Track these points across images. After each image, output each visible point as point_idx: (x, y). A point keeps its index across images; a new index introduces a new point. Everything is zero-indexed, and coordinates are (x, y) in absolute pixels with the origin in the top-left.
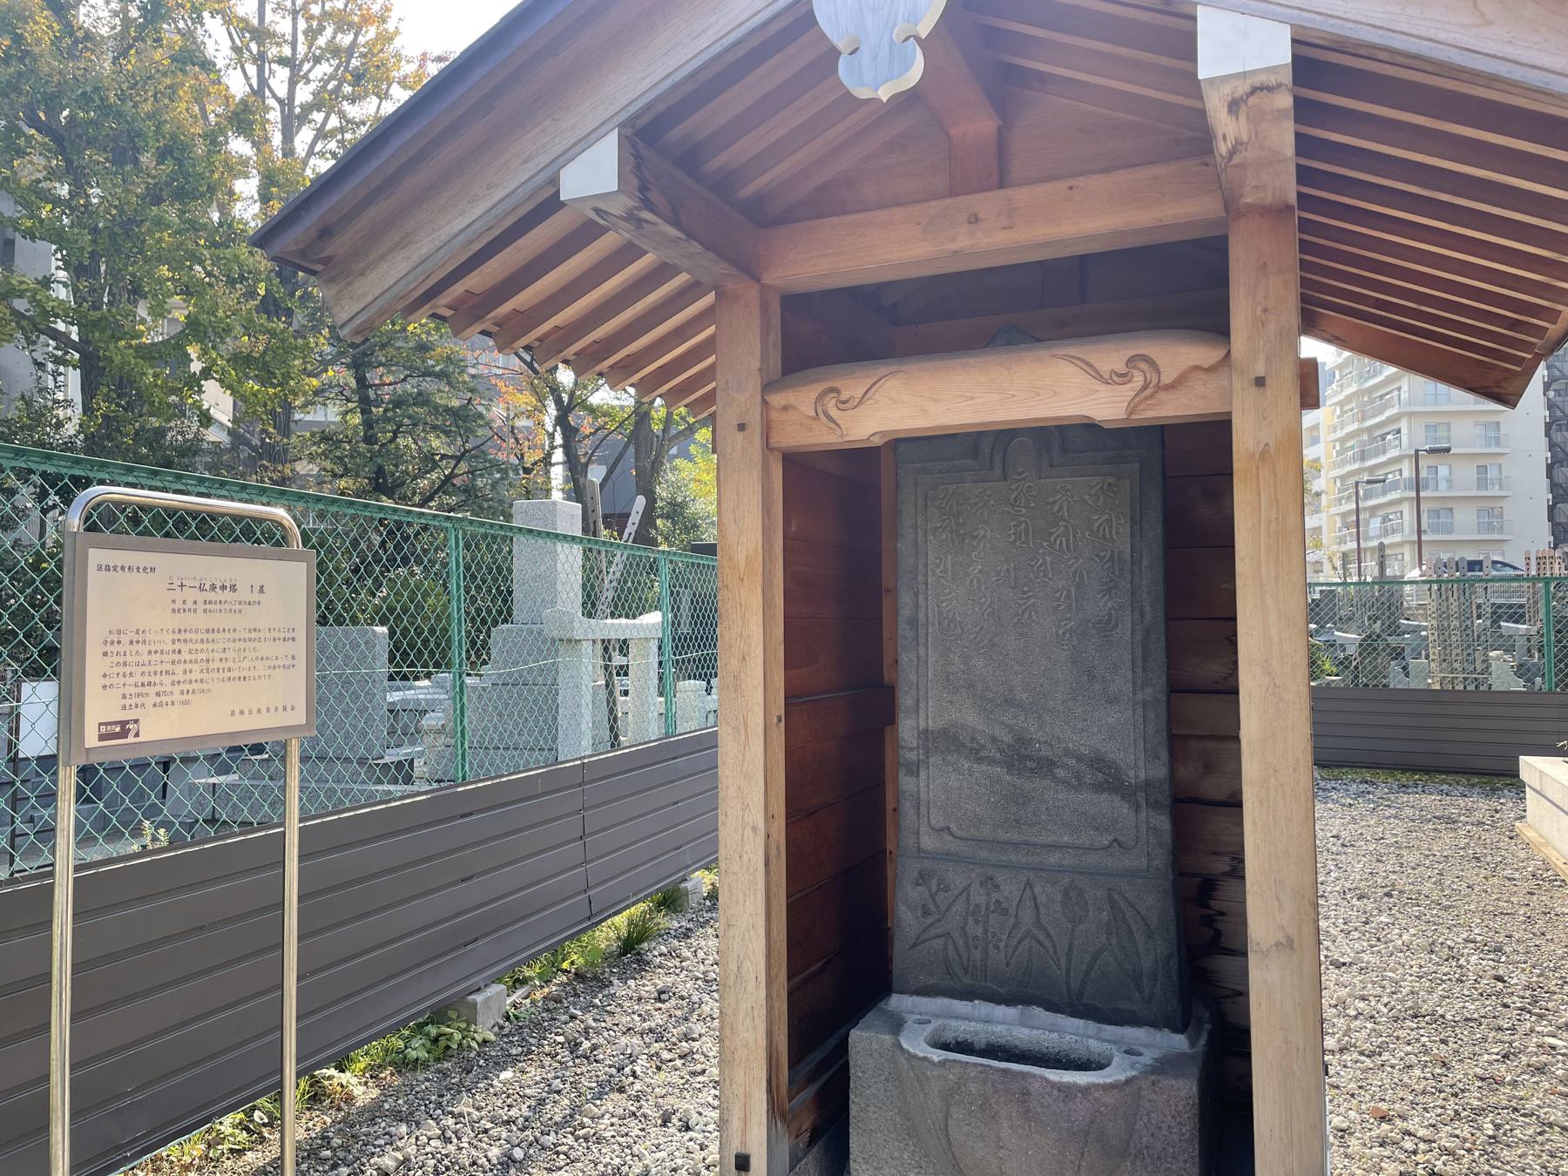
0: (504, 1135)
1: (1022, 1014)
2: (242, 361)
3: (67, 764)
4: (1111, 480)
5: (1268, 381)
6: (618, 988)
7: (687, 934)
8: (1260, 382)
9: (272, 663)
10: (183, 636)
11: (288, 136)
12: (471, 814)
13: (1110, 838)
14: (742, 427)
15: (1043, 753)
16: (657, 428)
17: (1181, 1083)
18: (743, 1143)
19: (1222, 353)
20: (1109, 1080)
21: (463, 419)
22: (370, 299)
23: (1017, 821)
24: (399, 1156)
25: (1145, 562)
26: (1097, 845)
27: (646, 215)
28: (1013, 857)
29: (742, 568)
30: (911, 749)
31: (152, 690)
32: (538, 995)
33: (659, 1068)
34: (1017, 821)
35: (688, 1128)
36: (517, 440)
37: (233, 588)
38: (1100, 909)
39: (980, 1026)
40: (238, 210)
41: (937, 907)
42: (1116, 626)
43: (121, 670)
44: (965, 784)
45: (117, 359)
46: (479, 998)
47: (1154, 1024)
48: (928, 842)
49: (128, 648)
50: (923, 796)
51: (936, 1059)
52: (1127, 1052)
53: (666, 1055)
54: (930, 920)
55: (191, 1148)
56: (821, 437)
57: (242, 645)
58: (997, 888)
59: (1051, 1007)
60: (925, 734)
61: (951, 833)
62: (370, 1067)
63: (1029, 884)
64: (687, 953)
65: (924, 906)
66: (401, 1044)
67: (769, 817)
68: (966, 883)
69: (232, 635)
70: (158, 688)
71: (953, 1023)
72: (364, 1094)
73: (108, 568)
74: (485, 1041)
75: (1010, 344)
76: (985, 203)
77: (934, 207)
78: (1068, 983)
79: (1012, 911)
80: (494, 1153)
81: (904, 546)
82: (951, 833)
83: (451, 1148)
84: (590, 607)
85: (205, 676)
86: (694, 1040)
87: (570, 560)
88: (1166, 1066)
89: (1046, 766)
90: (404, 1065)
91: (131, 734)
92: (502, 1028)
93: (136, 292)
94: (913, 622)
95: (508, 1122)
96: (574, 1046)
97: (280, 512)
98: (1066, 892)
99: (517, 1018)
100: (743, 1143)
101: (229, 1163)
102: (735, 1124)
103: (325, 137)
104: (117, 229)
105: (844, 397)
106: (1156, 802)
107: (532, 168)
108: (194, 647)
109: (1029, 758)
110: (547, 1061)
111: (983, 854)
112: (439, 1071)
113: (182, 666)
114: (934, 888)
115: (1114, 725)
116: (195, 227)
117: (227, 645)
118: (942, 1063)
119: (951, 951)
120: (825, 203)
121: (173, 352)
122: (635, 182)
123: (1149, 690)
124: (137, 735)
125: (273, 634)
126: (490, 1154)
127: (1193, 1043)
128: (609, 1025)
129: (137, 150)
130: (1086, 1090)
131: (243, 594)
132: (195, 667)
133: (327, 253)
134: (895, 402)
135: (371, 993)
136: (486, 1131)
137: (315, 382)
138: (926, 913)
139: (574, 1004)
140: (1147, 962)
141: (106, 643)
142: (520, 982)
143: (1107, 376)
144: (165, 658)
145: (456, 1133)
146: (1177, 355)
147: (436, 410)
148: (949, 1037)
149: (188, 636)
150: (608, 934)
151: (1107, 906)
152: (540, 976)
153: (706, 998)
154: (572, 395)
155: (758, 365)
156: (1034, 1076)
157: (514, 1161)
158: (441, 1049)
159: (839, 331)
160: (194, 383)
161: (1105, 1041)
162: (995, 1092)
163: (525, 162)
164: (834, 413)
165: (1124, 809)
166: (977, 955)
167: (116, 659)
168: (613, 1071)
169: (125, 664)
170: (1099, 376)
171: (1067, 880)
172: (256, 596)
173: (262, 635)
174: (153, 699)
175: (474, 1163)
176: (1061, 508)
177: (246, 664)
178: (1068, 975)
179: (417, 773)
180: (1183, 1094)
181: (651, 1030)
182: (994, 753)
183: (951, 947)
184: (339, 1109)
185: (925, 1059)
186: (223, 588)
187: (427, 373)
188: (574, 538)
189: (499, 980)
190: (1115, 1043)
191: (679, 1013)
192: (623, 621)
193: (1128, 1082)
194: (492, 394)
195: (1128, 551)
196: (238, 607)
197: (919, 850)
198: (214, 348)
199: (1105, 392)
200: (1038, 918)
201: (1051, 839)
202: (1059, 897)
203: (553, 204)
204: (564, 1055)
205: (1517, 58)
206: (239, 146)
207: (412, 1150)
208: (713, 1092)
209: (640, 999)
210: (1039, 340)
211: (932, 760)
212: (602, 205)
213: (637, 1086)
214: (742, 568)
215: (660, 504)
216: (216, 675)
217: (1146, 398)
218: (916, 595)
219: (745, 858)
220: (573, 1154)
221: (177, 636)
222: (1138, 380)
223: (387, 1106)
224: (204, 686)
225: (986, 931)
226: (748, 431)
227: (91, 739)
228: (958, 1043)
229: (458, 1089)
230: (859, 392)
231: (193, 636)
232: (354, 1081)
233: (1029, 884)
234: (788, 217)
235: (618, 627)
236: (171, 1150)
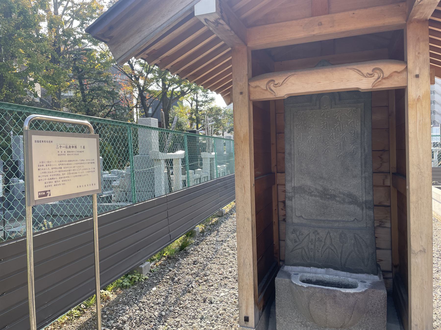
0: (158, 308)
1: (326, 271)
2: (46, 77)
3: (29, 205)
4: (354, 109)
5: (420, 76)
6: (181, 261)
7: (197, 244)
8: (417, 76)
9: (88, 171)
10: (62, 163)
11: (56, 9)
12: (138, 213)
13: (354, 218)
14: (241, 93)
16: (168, 97)
17: (381, 291)
18: (247, 313)
19: (403, 67)
20: (358, 292)
21: (112, 95)
22: (127, 50)
24: (127, 316)
25: (366, 134)
26: (350, 220)
27: (221, 21)
29: (242, 138)
30: (290, 193)
31: (53, 181)
32: (158, 264)
33: (199, 285)
35: (211, 303)
36: (127, 101)
37: (76, 147)
39: (314, 275)
40: (41, 31)
41: (299, 240)
42: (356, 154)
43: (44, 174)
44: (307, 203)
45: (9, 77)
46: (143, 266)
47: (368, 273)
48: (295, 220)
49: (46, 167)
50: (294, 206)
51: (305, 286)
52: (361, 282)
53: (200, 281)
54: (297, 244)
55: (64, 318)
56: (268, 96)
57: (79, 165)
58: (318, 234)
59: (336, 269)
60: (294, 188)
61: (303, 218)
62: (113, 289)
63: (329, 233)
64: (199, 250)
66: (121, 281)
67: (252, 215)
69: (76, 162)
70: (55, 180)
71: (305, 274)
72: (113, 297)
73: (38, 141)
74: (145, 279)
75: (323, 66)
76: (324, 19)
77: (307, 20)
78: (341, 261)
80: (156, 313)
82: (303, 218)
83: (143, 313)
84: (162, 149)
85: (69, 175)
86: (208, 276)
87: (155, 136)
88: (374, 286)
89: (333, 197)
90: (123, 287)
91: (48, 195)
92: (150, 274)
93: (13, 56)
94: (290, 154)
95: (158, 304)
96: (173, 279)
97: (86, 122)
99: (153, 271)
100: (247, 313)
101: (75, 321)
102: (244, 308)
103: (67, 10)
104: (7, 37)
105: (276, 83)
107: (184, 5)
108: (65, 166)
109: (328, 194)
110: (165, 284)
112: (133, 288)
113: (62, 173)
114: (298, 234)
115: (355, 184)
116: (31, 36)
117: (75, 165)
118: (308, 288)
119: (304, 253)
120: (267, 20)
121: (23, 75)
122: (220, 10)
123: (367, 173)
124: (50, 195)
125: (88, 162)
126: (155, 314)
127: (380, 279)
128: (182, 272)
129: (11, 13)
130: (354, 294)
131: (79, 149)
132: (66, 173)
133: (111, 35)
134: (293, 84)
135: (113, 267)
136: (152, 307)
137: (68, 83)
139: (169, 266)
141: (39, 166)
142: (152, 260)
143: (365, 75)
144: (57, 170)
145: (143, 308)
146: (389, 68)
147: (104, 92)
148: (304, 278)
149: (63, 163)
150: (176, 244)
152: (158, 258)
153: (208, 263)
154: (143, 87)
155: (247, 73)
156: (337, 291)
157: (163, 316)
158: (133, 282)
159: (268, 62)
160: (32, 84)
161: (353, 278)
162: (325, 296)
163: (182, 2)
164: (273, 88)
165: (358, 210)
166: (312, 254)
167: (42, 171)
168: (186, 286)
169: (45, 172)
170: (363, 75)
171: (341, 231)
172: (82, 150)
173: (85, 162)
174: (54, 183)
175: (151, 317)
176: (338, 118)
177: (81, 171)
178: (341, 259)
179: (113, 198)
180: (382, 294)
181: (194, 273)
182: (316, 193)
183: (303, 251)
184: (106, 302)
185: (302, 286)
186: (73, 147)
187: (101, 81)
188: (157, 129)
189: (147, 261)
190: (357, 279)
191: (201, 268)
192: (172, 153)
193: (366, 291)
194: (119, 86)
196: (77, 153)
197: (293, 223)
198: (38, 73)
199: (365, 80)
201: (335, 219)
203: (192, 15)
204: (170, 282)
206: (41, 12)
207: (131, 314)
208: (216, 291)
209: (188, 264)
210: (333, 65)
211: (296, 196)
212: (208, 18)
213: (194, 291)
214: (242, 138)
215: (170, 119)
216: (72, 175)
217: (379, 82)
218: (291, 145)
219: (245, 229)
220: (180, 313)
221: (60, 163)
222: (376, 76)
223: (120, 300)
224: (69, 179)
225: (315, 246)
226: (244, 94)
227: (36, 197)
228: (307, 280)
229: (141, 294)
230: (281, 81)
231: (65, 163)
232: (109, 293)
233: (329, 233)
234: (255, 24)
235: (170, 155)
236: (59, 319)
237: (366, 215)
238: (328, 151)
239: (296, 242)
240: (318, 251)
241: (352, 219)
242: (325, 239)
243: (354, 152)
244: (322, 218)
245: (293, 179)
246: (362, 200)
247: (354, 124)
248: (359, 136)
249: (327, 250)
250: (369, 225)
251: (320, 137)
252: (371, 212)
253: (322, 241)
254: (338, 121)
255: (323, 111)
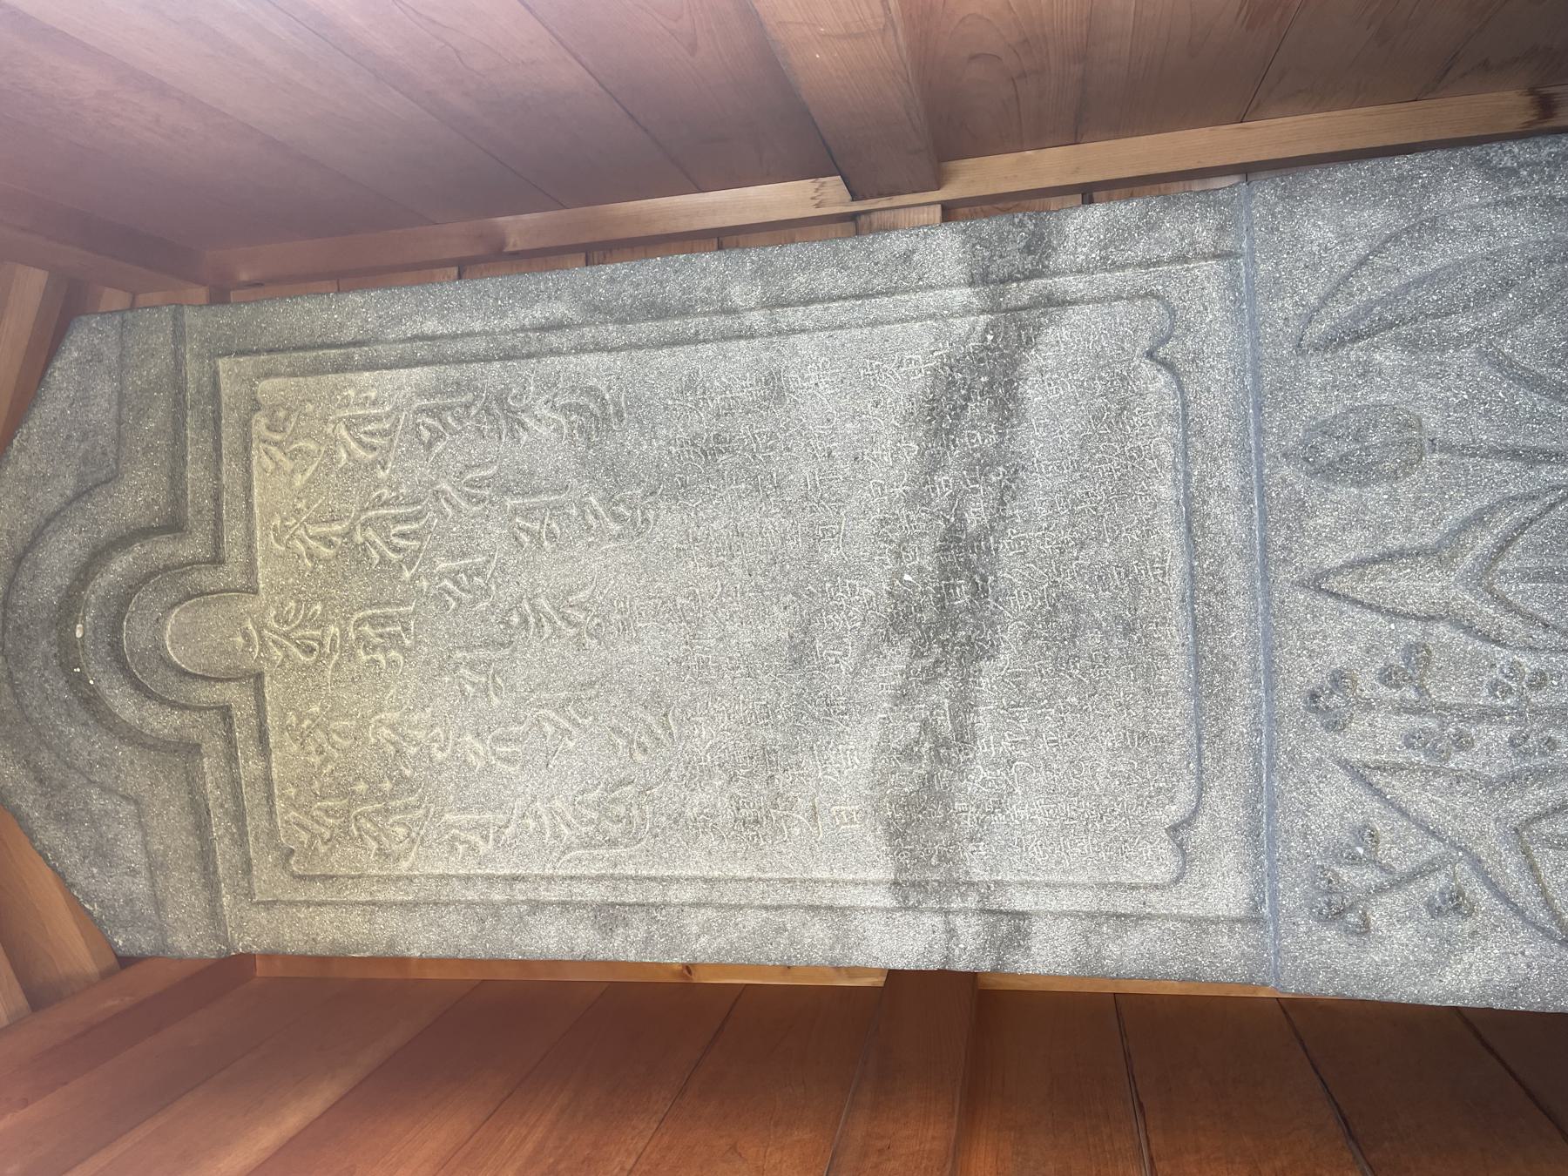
4: (260, 423)
13: (1147, 369)
15: (926, 562)
23: (1129, 630)
25: (431, 326)
26: (1172, 404)
28: (1237, 635)
34: (1129, 630)
38: (1366, 371)
42: (591, 391)
48: (1225, 890)
50: (1085, 901)
54: (1481, 895)
58: (1339, 680)
60: (908, 891)
61: (1188, 822)
63: (1316, 583)
65: (1436, 911)
68: (1342, 778)
79: (1412, 632)
81: (420, 939)
82: (1188, 822)
89: (963, 554)
94: (608, 916)
98: (1329, 472)
106: (1028, 249)
111: (1239, 725)
114: (1371, 877)
138: (1455, 903)
140: (1518, 231)
151: (1355, 352)
171: (1286, 471)
195: (417, 372)
197: (1253, 919)
200: (1422, 552)
201: (1170, 533)
202: (1345, 493)
205: (1192, 164)
211: (979, 874)
218: (537, 906)
225: (1484, 715)
233: (1316, 583)
237: (1108, 265)
238: (581, 607)
239: (1455, 903)
240: (1539, 681)
241: (1163, 378)
242: (1393, 614)
243: (579, 409)
244: (1174, 638)
245: (825, 896)
246: (967, 311)
247: (368, 419)
248: (453, 372)
249: (1509, 589)
250: (1203, 234)
251: (472, 666)
252: (1070, 229)
253: (1410, 649)
254: (348, 534)
255: (278, 655)
